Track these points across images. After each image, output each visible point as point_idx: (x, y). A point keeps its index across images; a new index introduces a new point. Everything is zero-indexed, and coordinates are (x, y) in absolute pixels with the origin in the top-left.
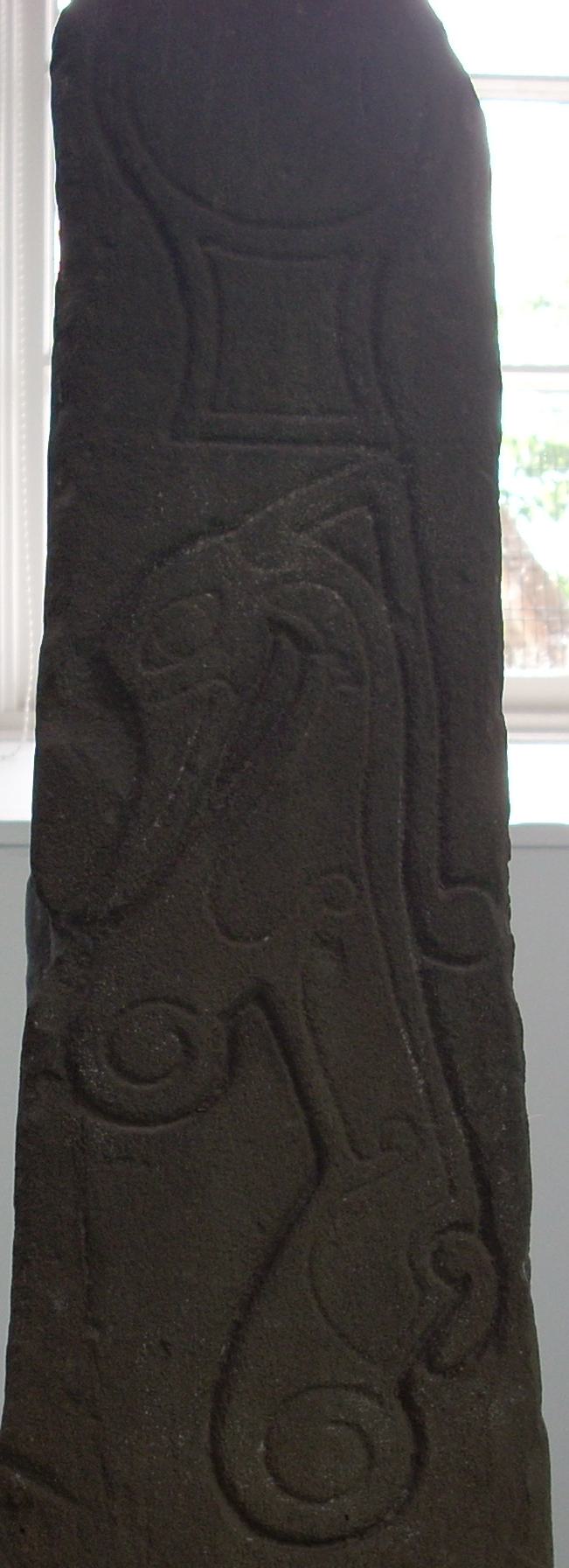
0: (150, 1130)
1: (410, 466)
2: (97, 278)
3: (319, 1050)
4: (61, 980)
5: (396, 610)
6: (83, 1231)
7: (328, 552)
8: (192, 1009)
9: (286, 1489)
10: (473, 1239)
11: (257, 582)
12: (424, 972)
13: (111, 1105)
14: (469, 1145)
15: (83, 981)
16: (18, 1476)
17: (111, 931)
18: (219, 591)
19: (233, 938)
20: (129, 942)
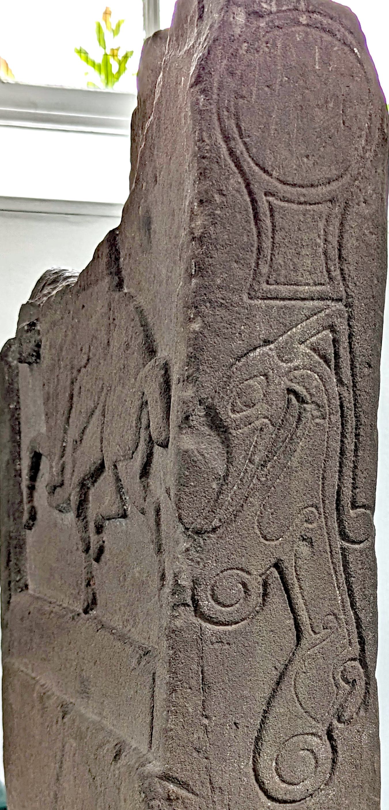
0: (229, 628)
1: (350, 310)
2: (216, 212)
3: (301, 588)
4: (188, 559)
5: (340, 382)
6: (201, 676)
7: (313, 354)
8: (248, 573)
9: (284, 781)
10: (357, 664)
11: (283, 371)
12: (343, 549)
13: (213, 618)
14: (356, 623)
15: (199, 560)
16: (172, 786)
17: (211, 535)
18: (265, 375)
19: (267, 540)
20: (221, 543)
